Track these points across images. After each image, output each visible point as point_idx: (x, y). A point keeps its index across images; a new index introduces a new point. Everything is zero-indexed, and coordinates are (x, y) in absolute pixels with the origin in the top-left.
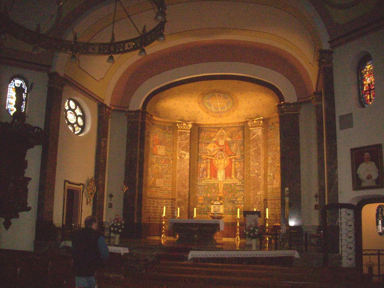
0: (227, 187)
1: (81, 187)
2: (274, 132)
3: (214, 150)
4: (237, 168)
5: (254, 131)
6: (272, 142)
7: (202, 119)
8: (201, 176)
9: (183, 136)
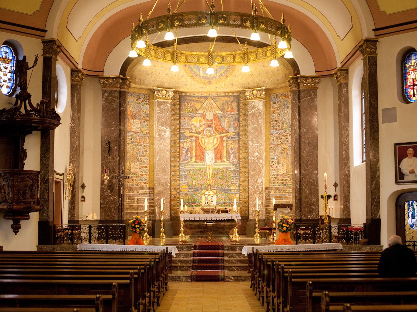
0: (219, 174)
2: (279, 106)
3: (201, 126)
4: (230, 149)
5: (253, 103)
6: (276, 118)
7: (186, 85)
8: (184, 159)
9: (162, 107)
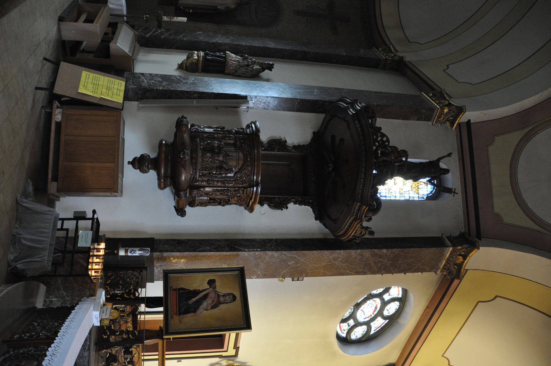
1: (232, 352)
